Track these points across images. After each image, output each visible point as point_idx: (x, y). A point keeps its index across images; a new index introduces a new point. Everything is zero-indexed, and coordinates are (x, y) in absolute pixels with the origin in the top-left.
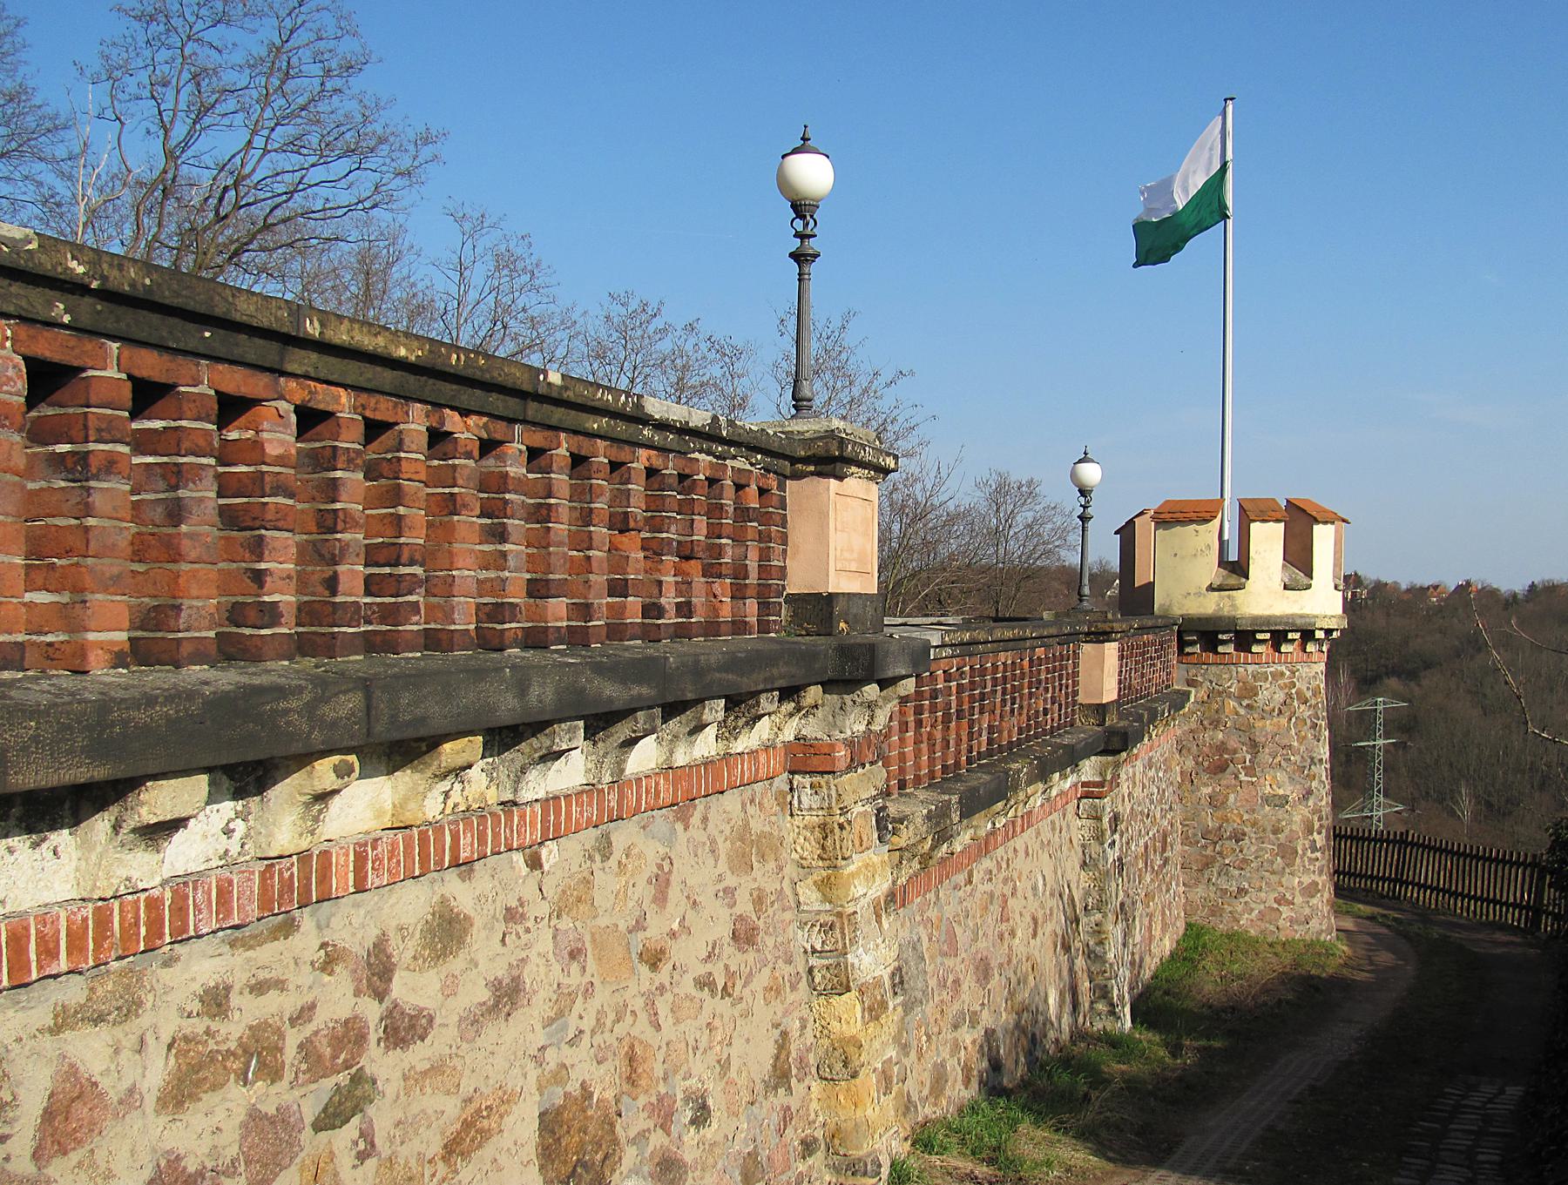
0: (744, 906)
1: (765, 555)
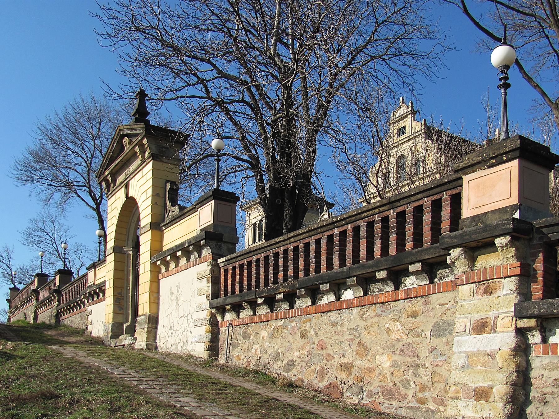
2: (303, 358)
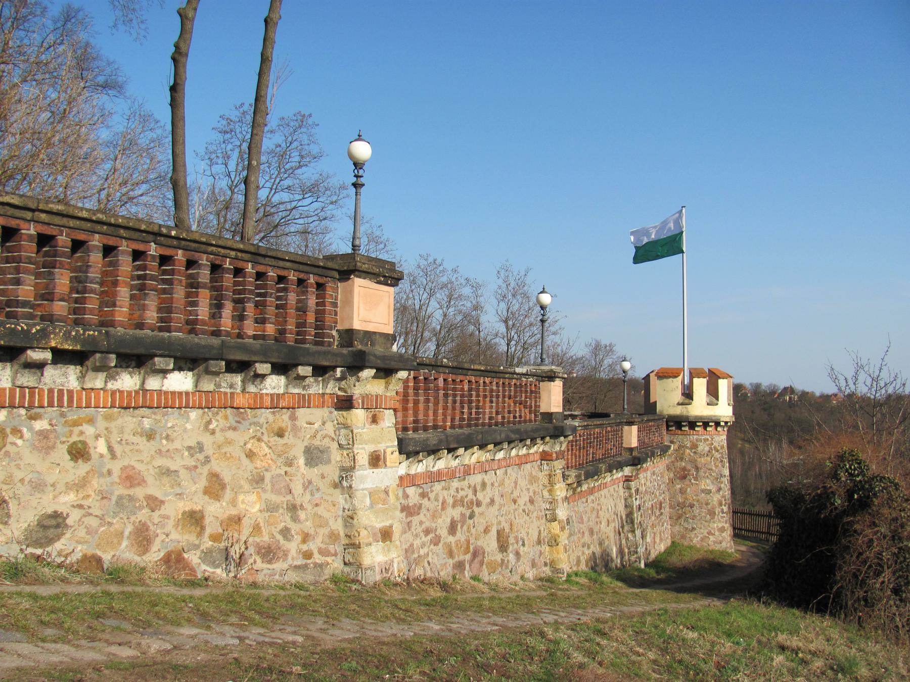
0: (531, 494)
1: (536, 402)
2: (89, 507)
